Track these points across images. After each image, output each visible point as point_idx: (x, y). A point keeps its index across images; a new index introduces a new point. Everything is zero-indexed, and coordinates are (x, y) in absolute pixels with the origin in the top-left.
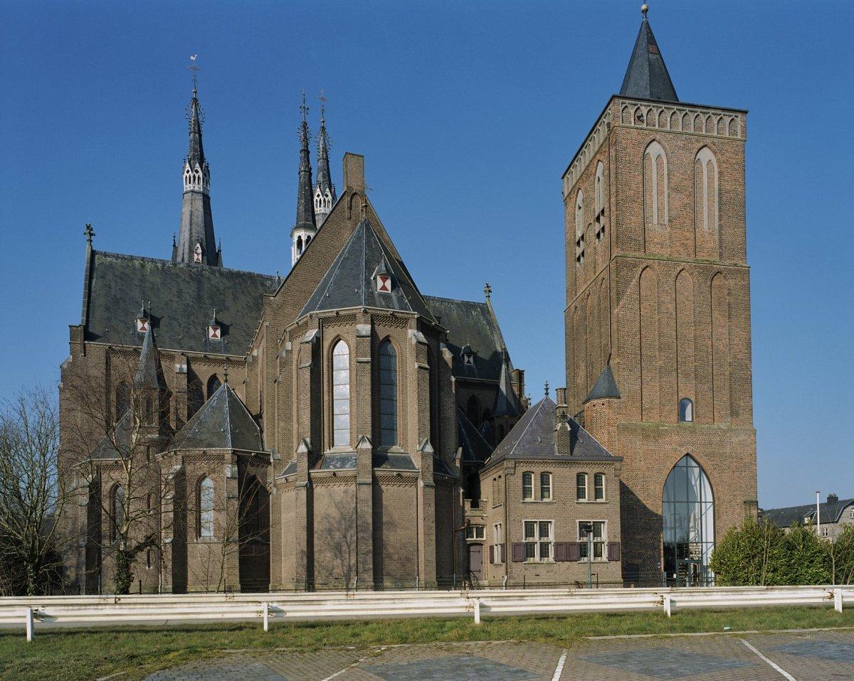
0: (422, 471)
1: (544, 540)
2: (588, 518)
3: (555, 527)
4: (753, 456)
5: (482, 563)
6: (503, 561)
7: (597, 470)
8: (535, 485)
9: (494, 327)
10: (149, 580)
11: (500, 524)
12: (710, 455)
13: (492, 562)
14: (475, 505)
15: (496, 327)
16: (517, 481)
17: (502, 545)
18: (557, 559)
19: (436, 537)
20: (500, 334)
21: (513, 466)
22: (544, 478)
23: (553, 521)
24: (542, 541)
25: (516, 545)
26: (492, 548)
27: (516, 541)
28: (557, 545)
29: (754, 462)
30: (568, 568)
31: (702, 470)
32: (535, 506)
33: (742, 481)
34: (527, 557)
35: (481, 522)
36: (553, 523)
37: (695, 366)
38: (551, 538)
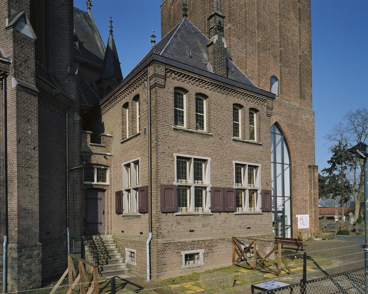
0: (15, 62)
1: (199, 184)
2: (244, 160)
3: (212, 168)
4: (313, 131)
5: (104, 213)
6: (142, 211)
7: (253, 105)
8: (189, 109)
9: (94, 30)
10: (340, 197)
11: (136, 163)
12: (290, 126)
13: (119, 211)
14: (96, 140)
15: (96, 30)
16: (167, 97)
17: (141, 190)
18: (214, 210)
19: (40, 174)
20: (100, 35)
21: (163, 74)
22: (200, 97)
23: (209, 159)
24: (196, 185)
25: (166, 189)
26: (119, 195)
27: (165, 183)
28: (215, 191)
29: (313, 137)
30: (225, 221)
31: (285, 140)
32: (188, 137)
33: (307, 150)
34: (179, 206)
35: (103, 161)
36: (209, 162)
37: (280, 50)
38: (206, 181)
